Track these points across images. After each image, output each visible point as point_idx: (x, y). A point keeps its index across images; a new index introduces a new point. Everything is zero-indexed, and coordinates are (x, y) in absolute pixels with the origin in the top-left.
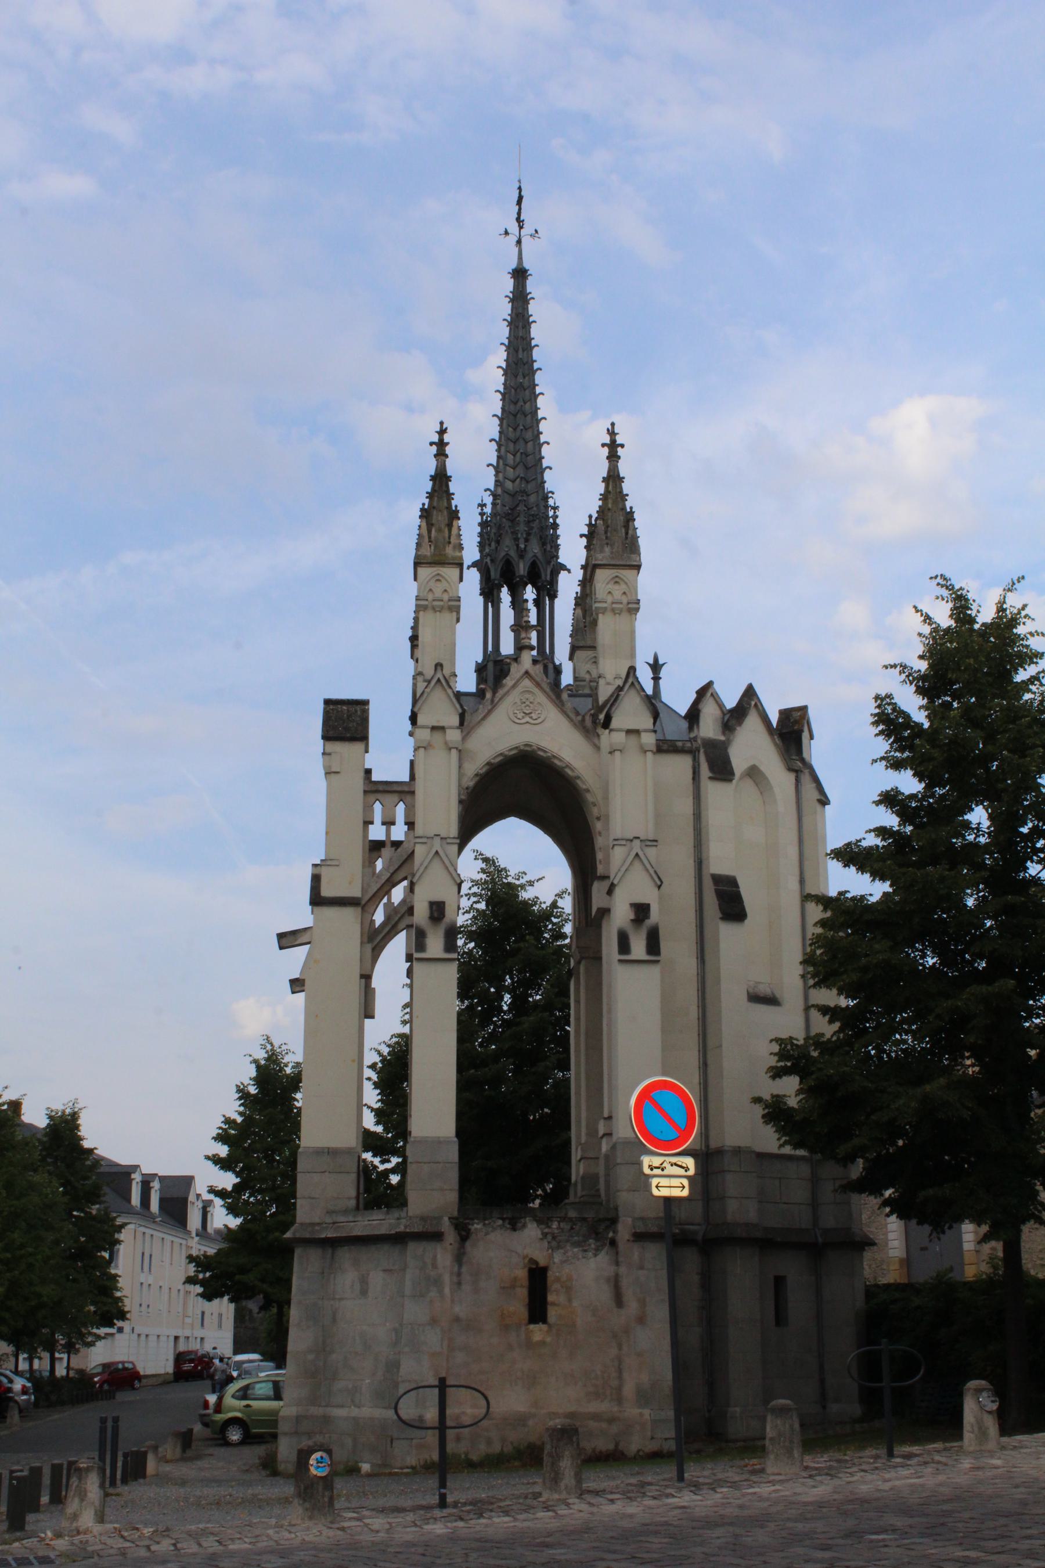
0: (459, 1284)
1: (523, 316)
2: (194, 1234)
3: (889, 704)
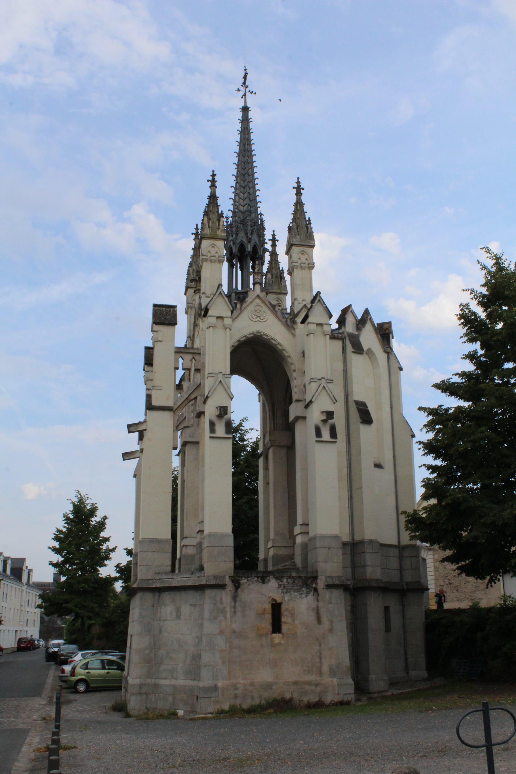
0: (235, 612)
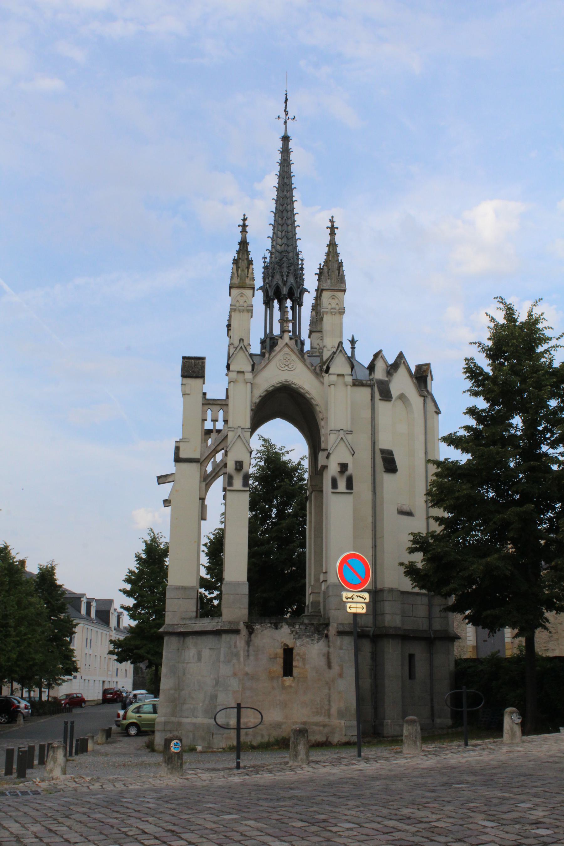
0: (248, 656)
1: (287, 161)
2: (113, 629)
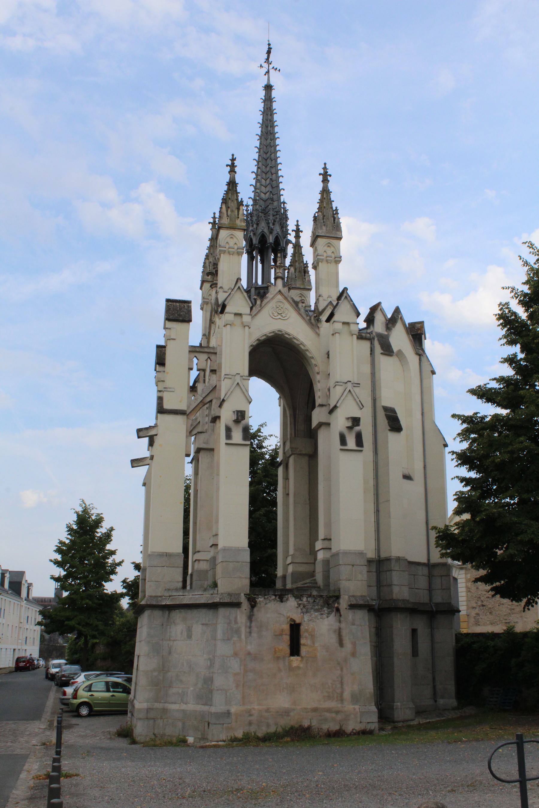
0: (250, 633)
2: (24, 600)
3: (506, 308)
